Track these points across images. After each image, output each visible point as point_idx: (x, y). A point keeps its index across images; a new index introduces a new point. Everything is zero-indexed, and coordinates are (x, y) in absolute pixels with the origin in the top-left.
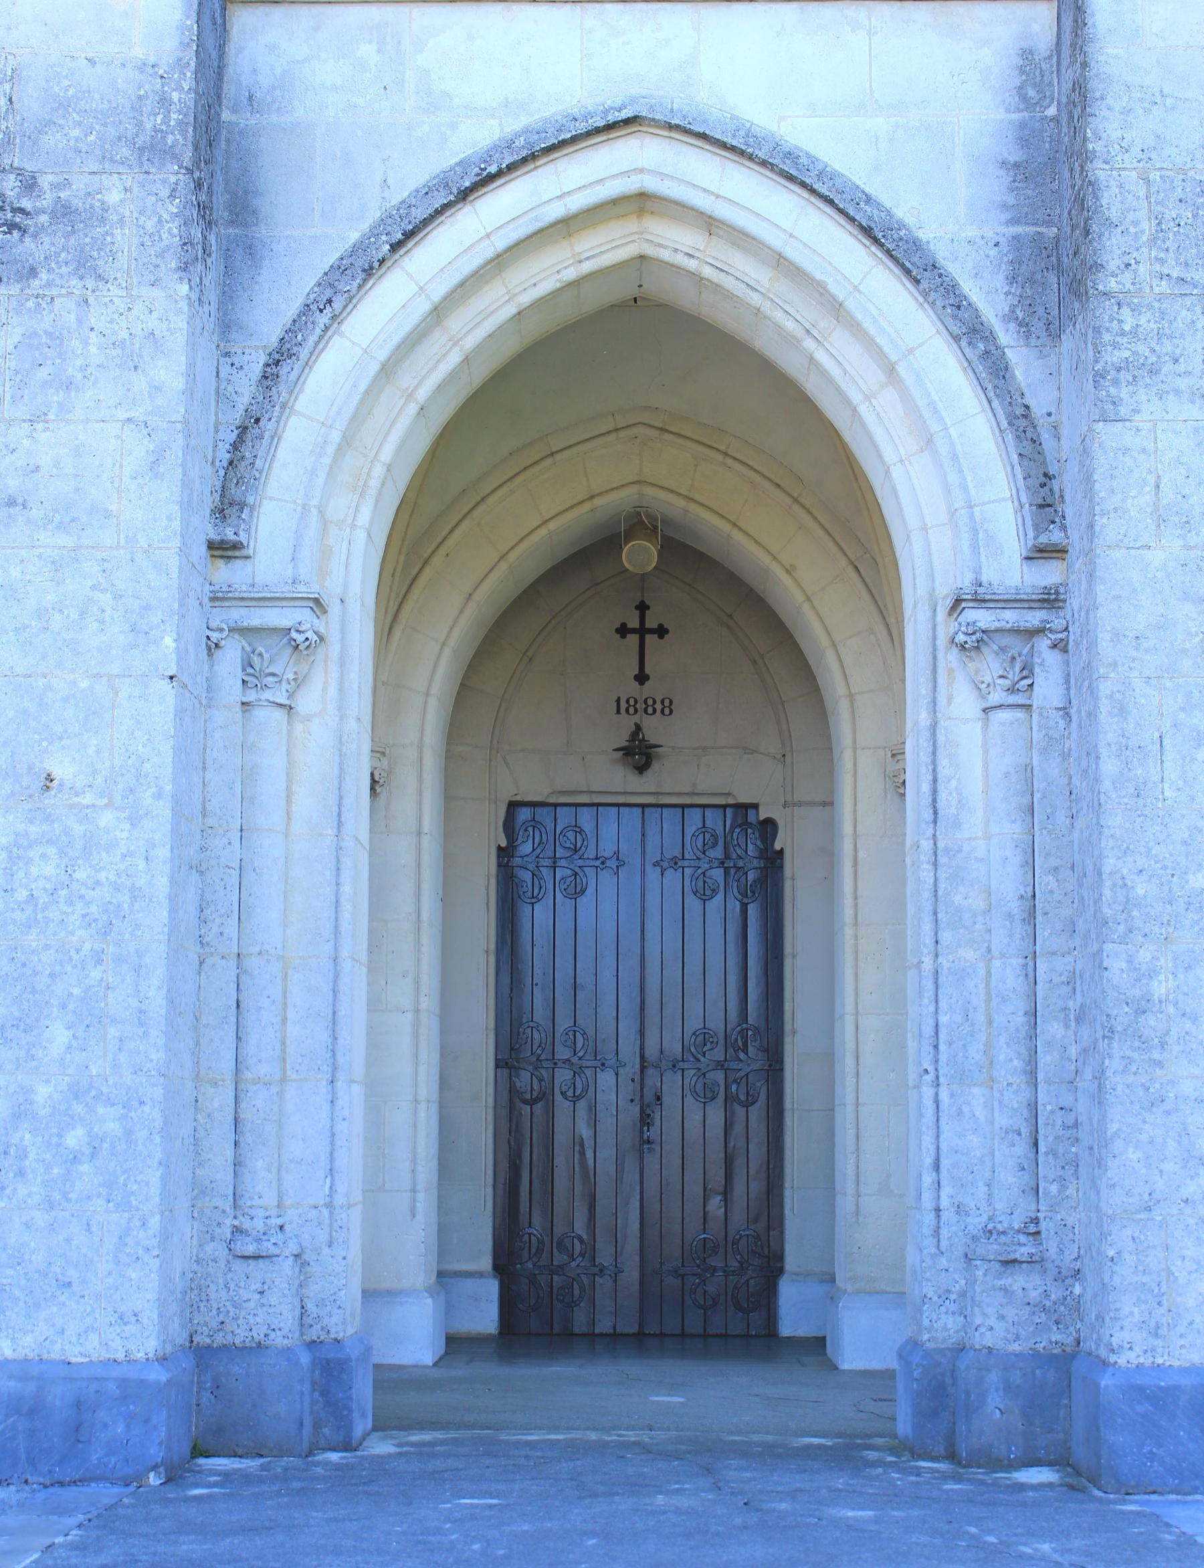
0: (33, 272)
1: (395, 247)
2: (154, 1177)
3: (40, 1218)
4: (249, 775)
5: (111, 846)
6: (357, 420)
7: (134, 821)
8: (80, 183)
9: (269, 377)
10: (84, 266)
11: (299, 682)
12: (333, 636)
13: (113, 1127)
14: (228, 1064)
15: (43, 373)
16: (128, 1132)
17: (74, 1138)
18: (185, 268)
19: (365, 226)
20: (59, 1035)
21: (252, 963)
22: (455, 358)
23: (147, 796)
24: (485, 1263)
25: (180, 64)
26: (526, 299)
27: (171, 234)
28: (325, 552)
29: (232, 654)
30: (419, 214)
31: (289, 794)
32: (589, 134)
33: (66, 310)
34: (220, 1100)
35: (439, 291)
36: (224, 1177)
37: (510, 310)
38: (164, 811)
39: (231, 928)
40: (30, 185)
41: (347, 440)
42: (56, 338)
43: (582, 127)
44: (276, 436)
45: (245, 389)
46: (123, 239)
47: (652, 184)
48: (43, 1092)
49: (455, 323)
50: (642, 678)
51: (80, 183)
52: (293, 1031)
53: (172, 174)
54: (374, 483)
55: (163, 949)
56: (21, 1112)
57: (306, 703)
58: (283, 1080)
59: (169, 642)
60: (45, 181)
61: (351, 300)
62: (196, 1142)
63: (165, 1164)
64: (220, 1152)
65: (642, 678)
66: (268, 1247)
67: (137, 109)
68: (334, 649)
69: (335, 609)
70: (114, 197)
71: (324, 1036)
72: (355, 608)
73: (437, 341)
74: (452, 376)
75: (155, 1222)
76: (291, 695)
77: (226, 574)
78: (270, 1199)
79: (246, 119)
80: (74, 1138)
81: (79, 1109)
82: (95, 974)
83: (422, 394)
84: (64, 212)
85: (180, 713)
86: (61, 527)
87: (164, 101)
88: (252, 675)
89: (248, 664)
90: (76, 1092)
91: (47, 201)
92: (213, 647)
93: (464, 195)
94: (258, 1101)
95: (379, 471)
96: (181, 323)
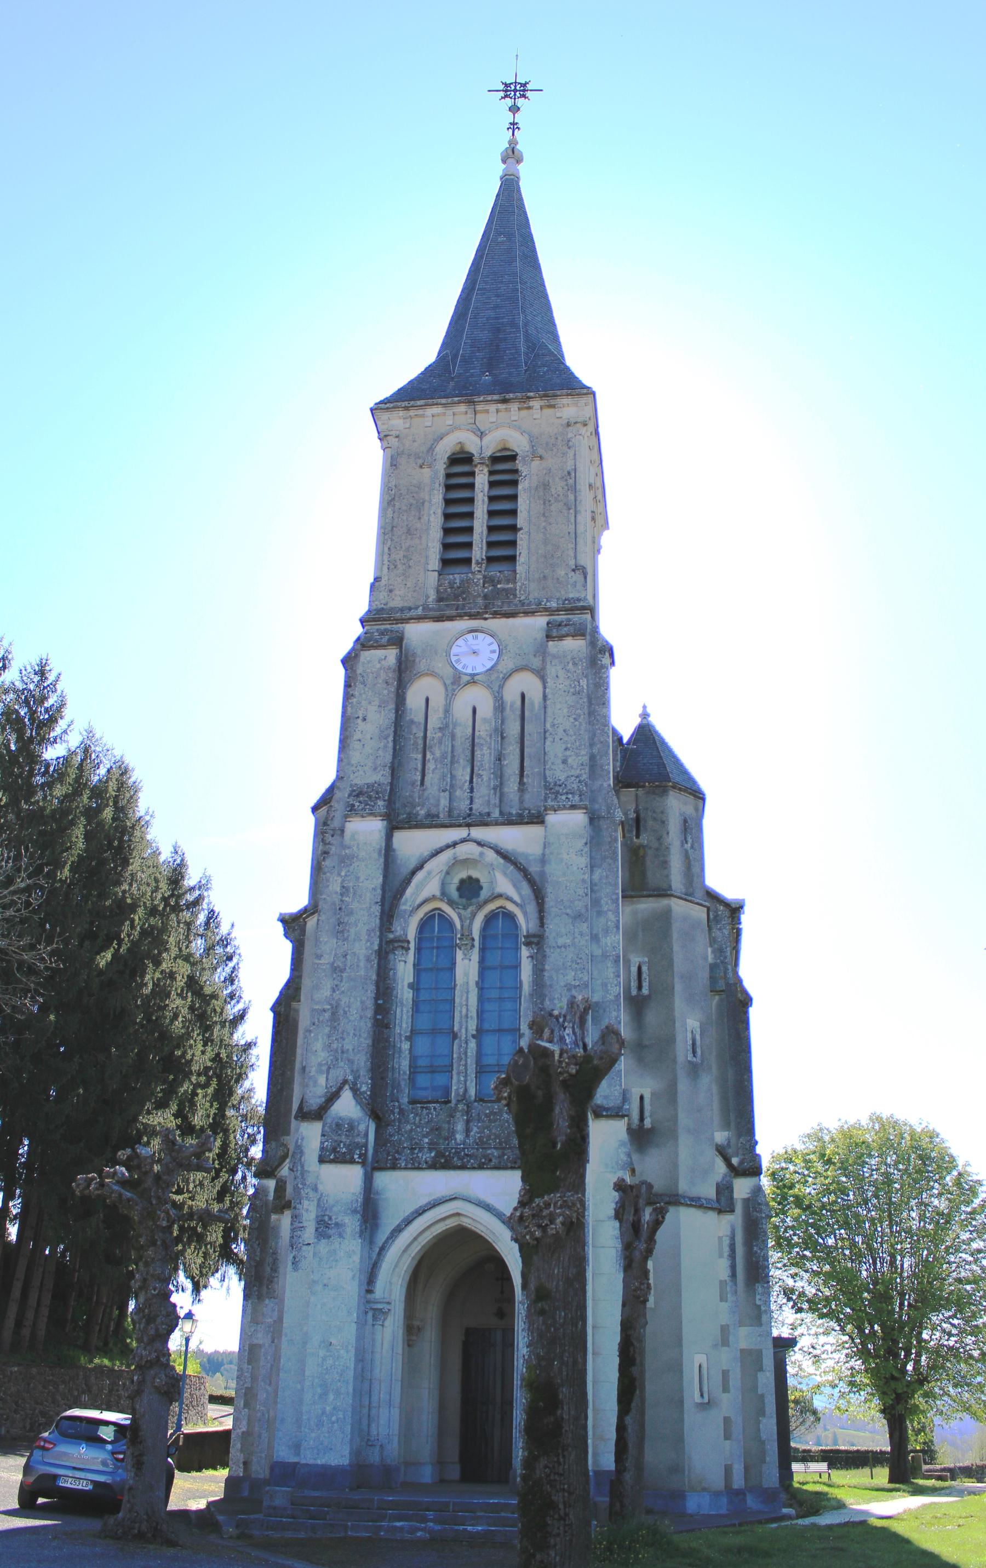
0: (330, 1237)
1: (406, 1226)
2: (349, 1427)
3: (327, 1435)
4: (373, 1340)
5: (343, 1357)
6: (398, 1262)
7: (347, 1352)
8: (340, 1218)
9: (379, 1254)
10: (341, 1236)
11: (385, 1319)
12: (393, 1308)
13: (341, 1416)
14: (367, 1403)
15: (332, 1258)
16: (344, 1418)
17: (334, 1419)
18: (360, 1236)
19: (400, 1220)
20: (331, 1397)
21: (373, 1381)
22: (419, 1247)
23: (350, 1347)
24: (456, 1459)
25: (360, 1193)
26: (435, 1234)
27: (358, 1229)
28: (391, 1290)
29: (370, 1314)
30: (411, 1219)
31: (382, 1344)
32: (447, 1201)
33: (336, 1245)
34: (365, 1411)
35: (415, 1235)
36: (365, 1428)
37: (431, 1237)
38: (353, 1351)
39: (369, 1374)
40: (330, 1218)
41: (396, 1266)
42: (335, 1251)
43: (448, 1198)
44: (381, 1266)
45: (374, 1256)
46: (348, 1230)
47: (460, 1211)
48: (328, 1408)
49: (420, 1239)
50: (502, 1292)
51: (340, 1218)
52: (382, 1396)
53: (358, 1216)
54: (402, 1275)
55: (352, 1379)
56: (324, 1413)
57: (387, 1323)
58: (379, 1406)
59: (355, 1315)
60: (333, 1218)
61: (396, 1237)
62: (360, 1419)
63: (352, 1424)
64: (365, 1422)
65: (502, 1292)
66: (374, 1443)
67: (352, 1202)
68: (393, 1312)
69: (393, 1303)
70: (347, 1221)
71: (388, 1397)
72: (397, 1303)
73: (416, 1243)
74: (418, 1252)
75: (349, 1436)
76: (383, 1322)
77: (369, 1296)
78: (375, 1433)
79: (376, 1197)
80: (334, 1419)
81: (335, 1412)
82: (339, 1384)
83: (412, 1255)
84: (337, 1224)
85: (357, 1330)
86: (335, 1290)
87: (357, 1201)
88: (375, 1318)
89: (373, 1316)
90: (334, 1408)
91: (333, 1222)
92: (366, 1313)
93: (420, 1214)
94: (374, 1412)
95: (403, 1272)
96: (359, 1248)
